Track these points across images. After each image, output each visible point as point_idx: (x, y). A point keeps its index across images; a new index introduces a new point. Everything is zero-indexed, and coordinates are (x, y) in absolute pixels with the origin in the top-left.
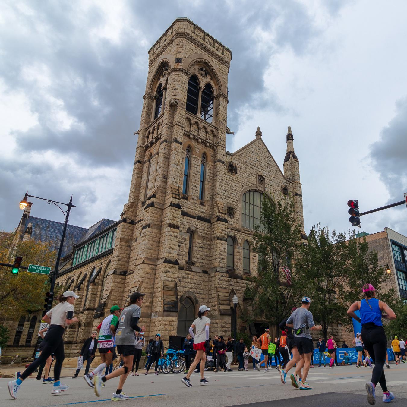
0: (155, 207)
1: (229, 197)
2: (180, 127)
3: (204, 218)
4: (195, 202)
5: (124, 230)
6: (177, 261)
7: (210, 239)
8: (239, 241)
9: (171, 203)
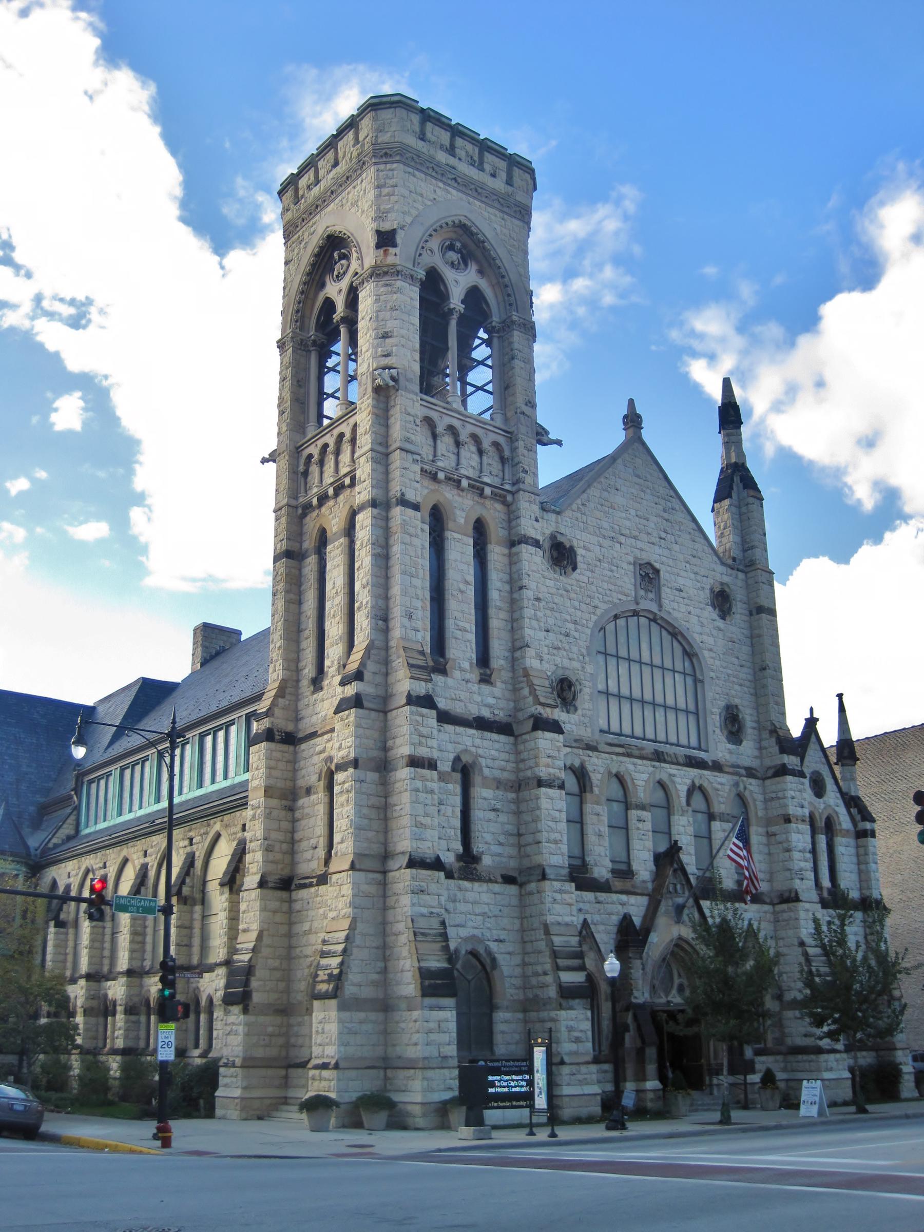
0: (367, 709)
1: (558, 648)
2: (410, 456)
3: (495, 722)
4: (468, 676)
5: (273, 763)
6: (438, 858)
7: (522, 785)
8: (596, 778)
9: (409, 696)
